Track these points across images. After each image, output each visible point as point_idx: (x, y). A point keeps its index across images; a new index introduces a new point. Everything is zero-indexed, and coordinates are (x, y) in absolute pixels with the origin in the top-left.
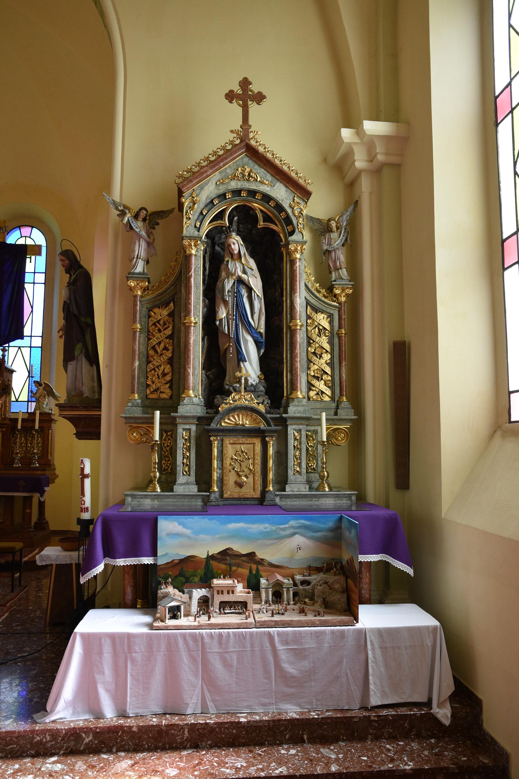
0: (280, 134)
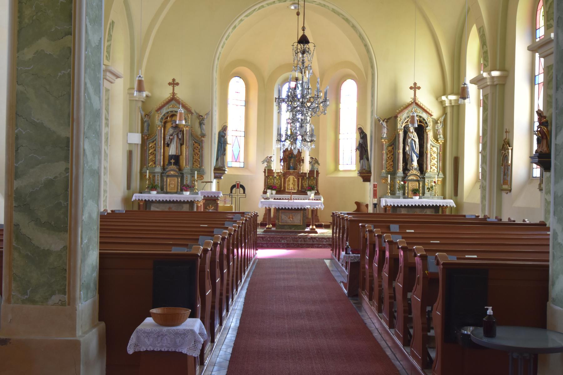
0: (426, 99)
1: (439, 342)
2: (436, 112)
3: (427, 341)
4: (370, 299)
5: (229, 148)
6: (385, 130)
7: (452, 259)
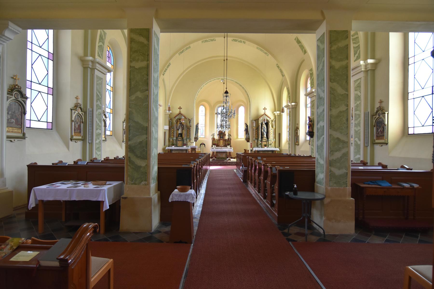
0: (269, 113)
1: (277, 197)
2: (272, 118)
3: (272, 197)
4: (251, 183)
5: (199, 130)
6: (254, 124)
7: (281, 168)
